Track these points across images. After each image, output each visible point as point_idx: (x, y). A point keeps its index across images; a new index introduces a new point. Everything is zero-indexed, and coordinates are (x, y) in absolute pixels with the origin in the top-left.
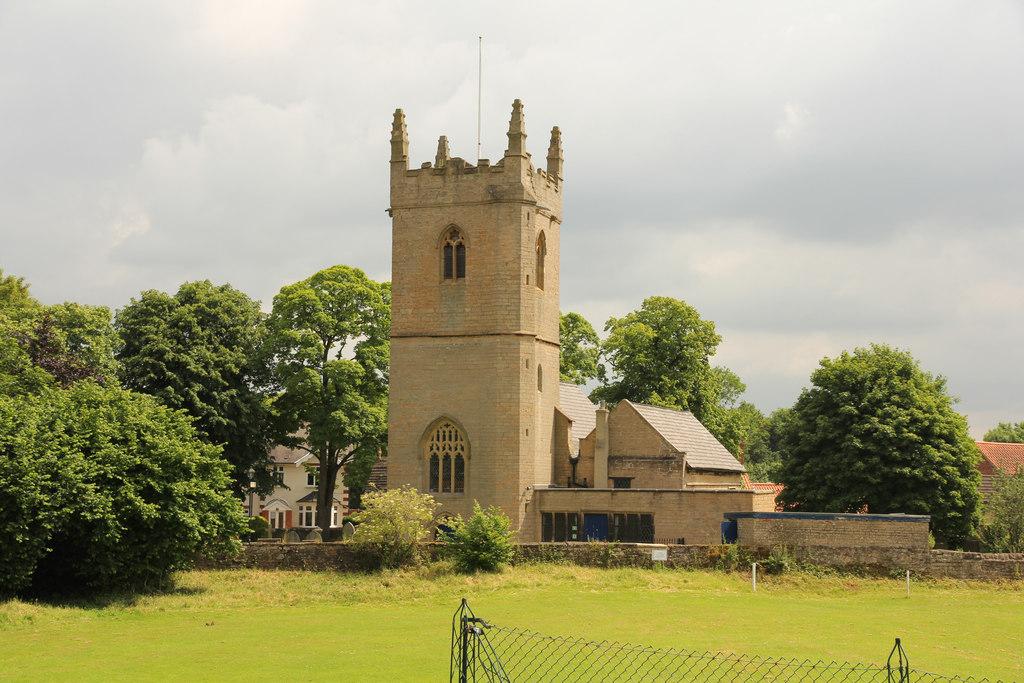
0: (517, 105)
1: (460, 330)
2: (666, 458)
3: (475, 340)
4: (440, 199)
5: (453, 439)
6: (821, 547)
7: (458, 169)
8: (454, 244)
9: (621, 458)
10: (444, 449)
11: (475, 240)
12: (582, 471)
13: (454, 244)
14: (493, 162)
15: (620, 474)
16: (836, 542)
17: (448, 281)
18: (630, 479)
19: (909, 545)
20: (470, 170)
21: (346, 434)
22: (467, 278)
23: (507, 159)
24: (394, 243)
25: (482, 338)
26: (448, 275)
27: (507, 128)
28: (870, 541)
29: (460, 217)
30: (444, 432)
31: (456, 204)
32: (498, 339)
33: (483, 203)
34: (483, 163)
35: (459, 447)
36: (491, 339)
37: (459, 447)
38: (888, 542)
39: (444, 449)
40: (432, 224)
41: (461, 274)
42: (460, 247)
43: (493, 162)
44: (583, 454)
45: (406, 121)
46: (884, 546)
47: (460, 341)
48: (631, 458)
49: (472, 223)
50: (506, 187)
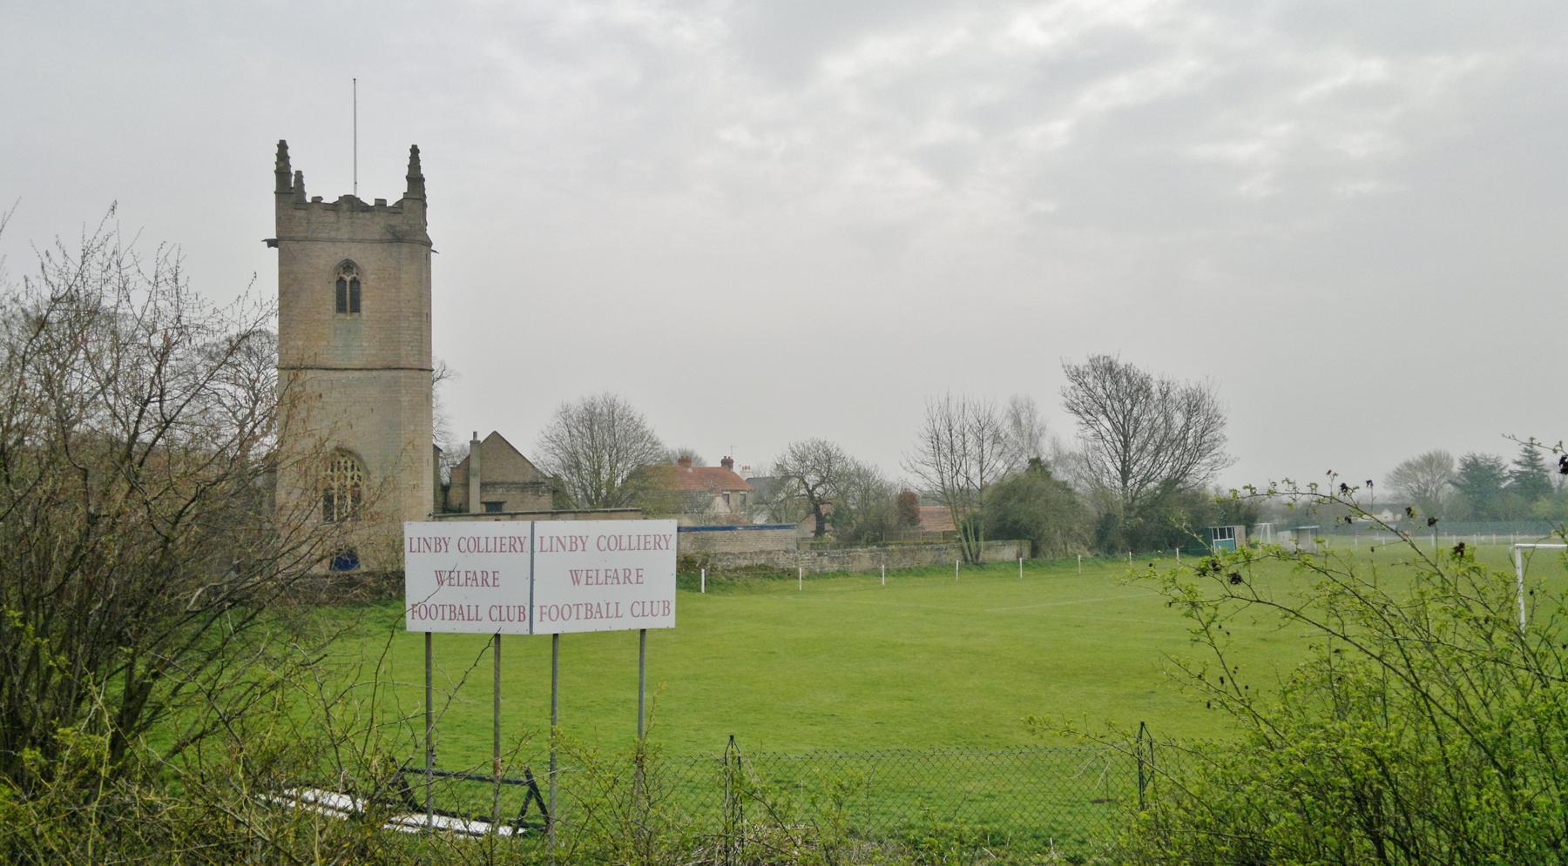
0: (415, 151)
1: (357, 363)
2: (534, 483)
3: (375, 373)
4: (333, 234)
5: (336, 470)
6: (726, 554)
7: (353, 206)
8: (348, 279)
9: (494, 485)
10: (352, 478)
11: (373, 276)
12: (455, 497)
13: (348, 279)
14: (390, 203)
15: (492, 498)
16: (736, 550)
17: (341, 316)
18: (501, 503)
19: (783, 548)
20: (366, 208)
21: (1282, 821)
22: (364, 313)
23: (406, 202)
24: (281, 275)
25: (381, 372)
26: (341, 308)
27: (406, 171)
28: (760, 546)
29: (356, 253)
30: (339, 463)
31: (352, 240)
32: (402, 373)
33: (381, 241)
34: (381, 203)
35: (356, 477)
36: (394, 373)
37: (356, 477)
38: (770, 547)
39: (352, 478)
40: (325, 258)
41: (356, 308)
42: (355, 282)
43: (390, 203)
44: (455, 480)
45: (290, 152)
46: (769, 549)
47: (357, 374)
48: (502, 483)
49: (370, 260)
50: (406, 228)
